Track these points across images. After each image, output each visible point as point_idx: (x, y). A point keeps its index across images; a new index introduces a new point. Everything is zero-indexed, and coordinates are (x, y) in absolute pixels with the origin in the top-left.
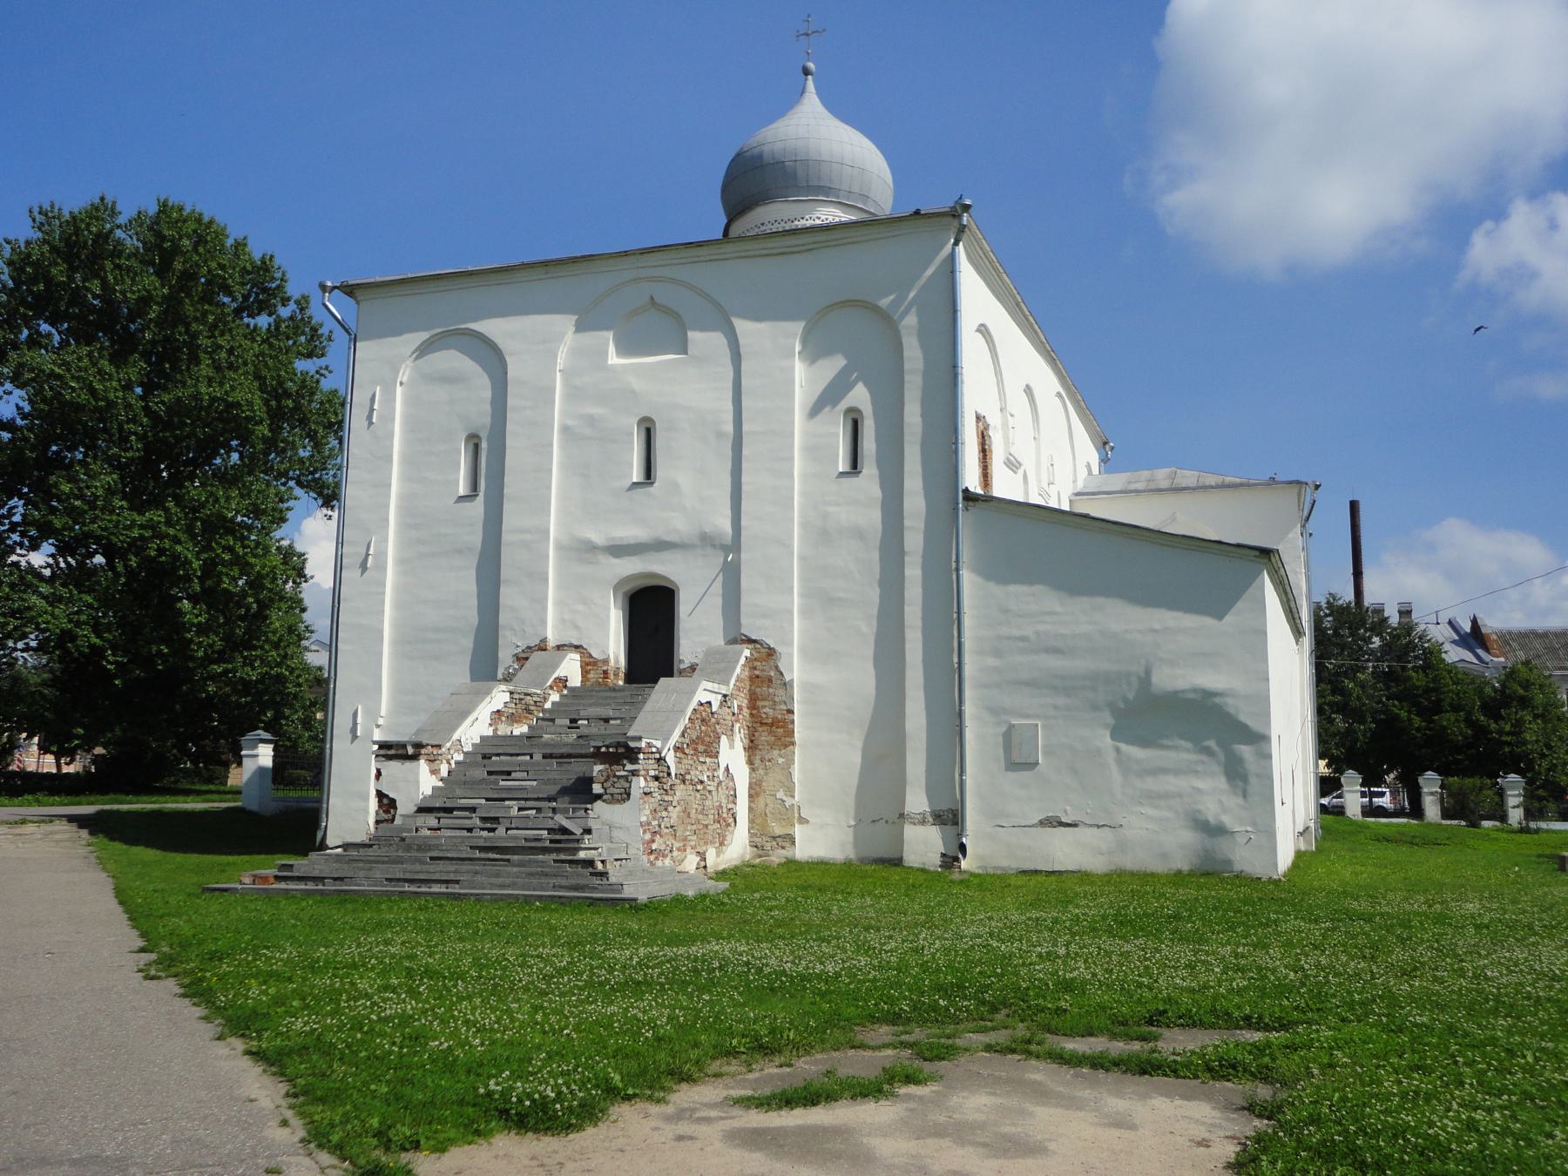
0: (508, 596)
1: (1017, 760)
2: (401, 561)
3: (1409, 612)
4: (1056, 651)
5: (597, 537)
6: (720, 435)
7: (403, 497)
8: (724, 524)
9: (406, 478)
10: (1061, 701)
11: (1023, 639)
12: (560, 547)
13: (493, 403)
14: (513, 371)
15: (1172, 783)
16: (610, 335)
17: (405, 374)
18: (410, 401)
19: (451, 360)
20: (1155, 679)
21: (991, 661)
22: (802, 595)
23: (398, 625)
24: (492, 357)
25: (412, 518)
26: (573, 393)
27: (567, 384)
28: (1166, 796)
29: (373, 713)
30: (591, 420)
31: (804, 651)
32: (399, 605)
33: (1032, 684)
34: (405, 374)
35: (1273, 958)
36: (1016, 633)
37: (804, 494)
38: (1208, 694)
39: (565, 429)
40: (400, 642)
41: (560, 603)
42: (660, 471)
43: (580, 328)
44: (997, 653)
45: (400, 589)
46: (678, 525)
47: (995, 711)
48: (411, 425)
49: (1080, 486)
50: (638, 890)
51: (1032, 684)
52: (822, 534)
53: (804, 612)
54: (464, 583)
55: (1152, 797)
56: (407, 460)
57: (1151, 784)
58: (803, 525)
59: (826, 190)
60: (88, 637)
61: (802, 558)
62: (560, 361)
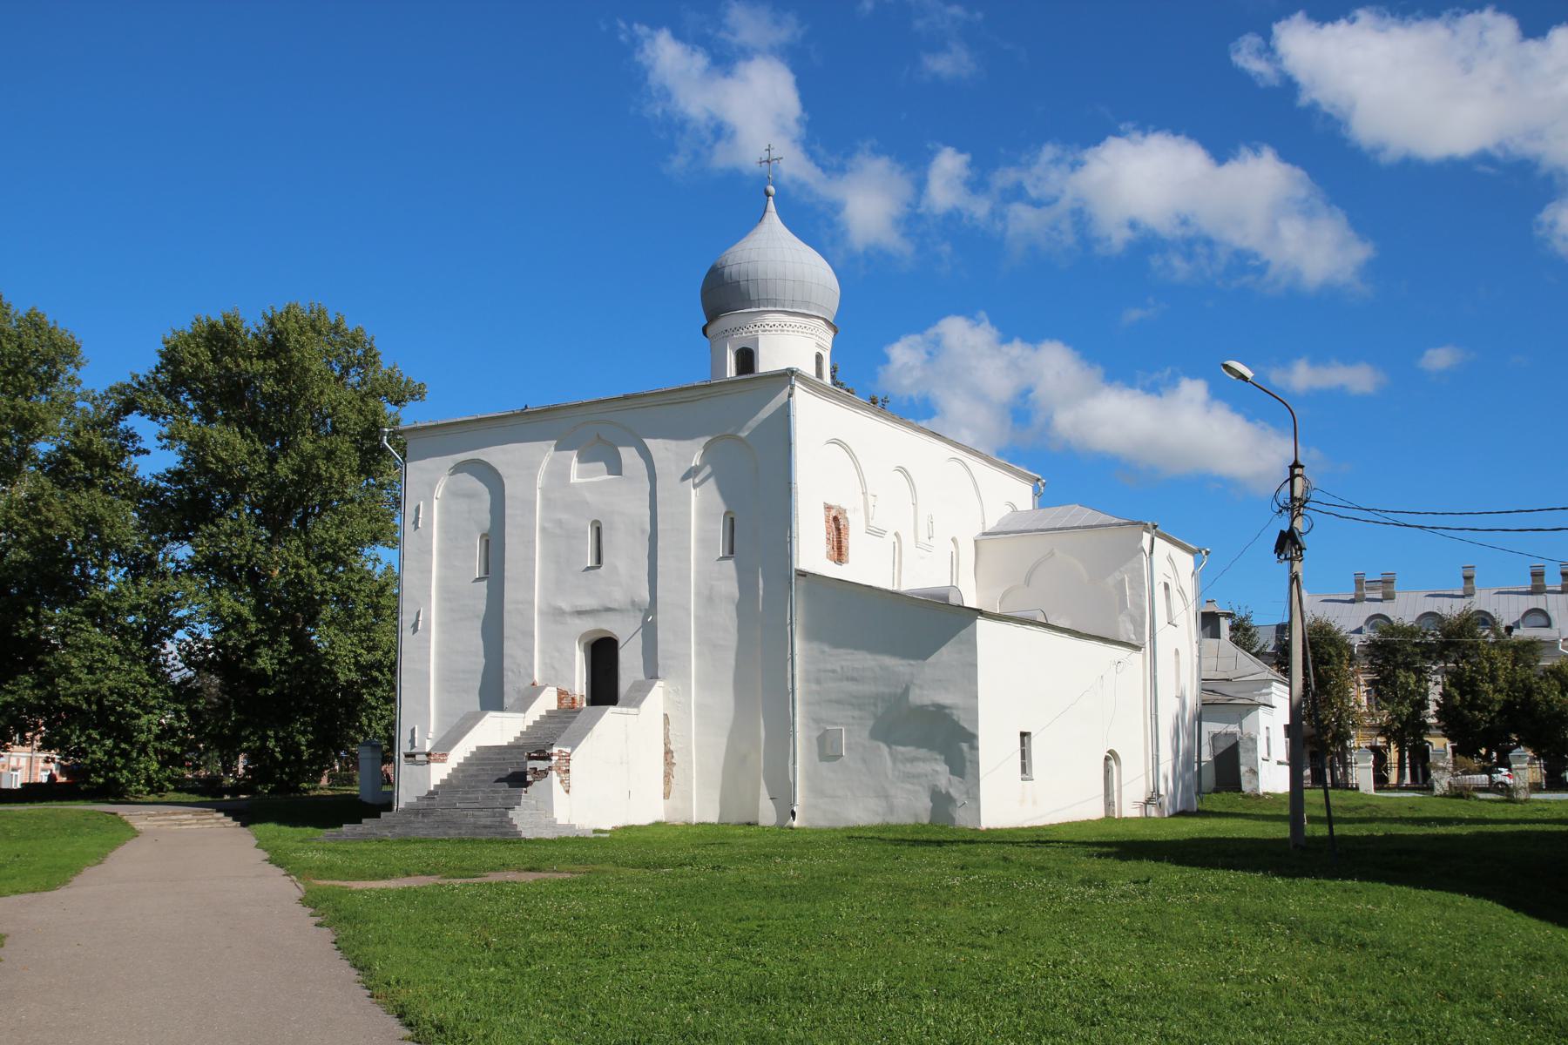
0: (509, 647)
1: (827, 750)
2: (440, 624)
3: (1542, 574)
4: (853, 679)
5: (565, 605)
6: (643, 531)
7: (441, 579)
8: (645, 595)
9: (442, 566)
10: (856, 713)
11: (834, 671)
12: (541, 613)
13: (492, 511)
14: (509, 490)
15: (922, 767)
16: (575, 452)
17: (439, 491)
18: (445, 510)
19: (469, 481)
20: (911, 698)
21: (814, 687)
22: (698, 644)
23: (439, 669)
24: (492, 478)
25: (447, 594)
26: (548, 502)
27: (545, 498)
28: (918, 776)
29: (425, 731)
30: (560, 523)
31: (698, 681)
32: (440, 655)
33: (839, 702)
34: (439, 491)
35: (818, 862)
36: (829, 667)
37: (698, 573)
38: (940, 708)
39: (543, 529)
40: (444, 680)
41: (542, 652)
42: (605, 559)
43: (557, 448)
44: (818, 682)
45: (439, 643)
46: (618, 597)
47: (817, 721)
48: (445, 528)
49: (991, 525)
50: (526, 834)
51: (839, 702)
52: (708, 599)
53: (698, 655)
54: (474, 641)
55: (909, 777)
56: (442, 553)
57: (909, 768)
58: (698, 594)
59: (768, 302)
60: (722, 35)
61: (697, 618)
62: (542, 474)
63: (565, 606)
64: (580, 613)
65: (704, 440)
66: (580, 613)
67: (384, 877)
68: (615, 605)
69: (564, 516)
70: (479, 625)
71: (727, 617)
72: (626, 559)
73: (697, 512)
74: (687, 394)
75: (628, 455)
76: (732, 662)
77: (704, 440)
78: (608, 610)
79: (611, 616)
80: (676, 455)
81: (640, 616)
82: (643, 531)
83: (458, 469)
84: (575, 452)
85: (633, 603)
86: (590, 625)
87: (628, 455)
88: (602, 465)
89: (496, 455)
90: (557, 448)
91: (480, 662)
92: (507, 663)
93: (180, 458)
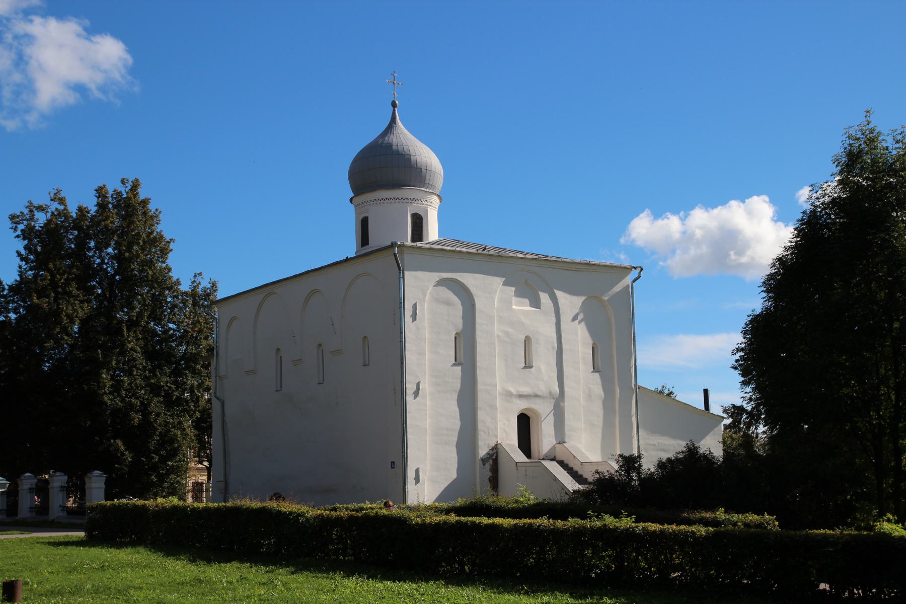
0: (481, 415)
8: (556, 389)
11: (654, 445)
14: (479, 305)
19: (447, 294)
43: (505, 284)
46: (542, 389)
63: (514, 391)
64: (521, 396)
65: (584, 298)
66: (521, 396)
67: (21, 540)
68: (539, 393)
69: (510, 330)
70: (455, 396)
71: (598, 408)
72: (545, 363)
73: (579, 340)
74: (574, 266)
75: (544, 298)
76: (600, 435)
77: (584, 298)
78: (536, 396)
79: (537, 400)
80: (570, 303)
81: (553, 401)
82: (553, 348)
83: (441, 283)
84: (513, 289)
85: (550, 393)
86: (521, 406)
87: (544, 298)
88: (527, 301)
89: (470, 280)
90: (505, 284)
91: (456, 424)
92: (480, 426)
93: (810, 207)
